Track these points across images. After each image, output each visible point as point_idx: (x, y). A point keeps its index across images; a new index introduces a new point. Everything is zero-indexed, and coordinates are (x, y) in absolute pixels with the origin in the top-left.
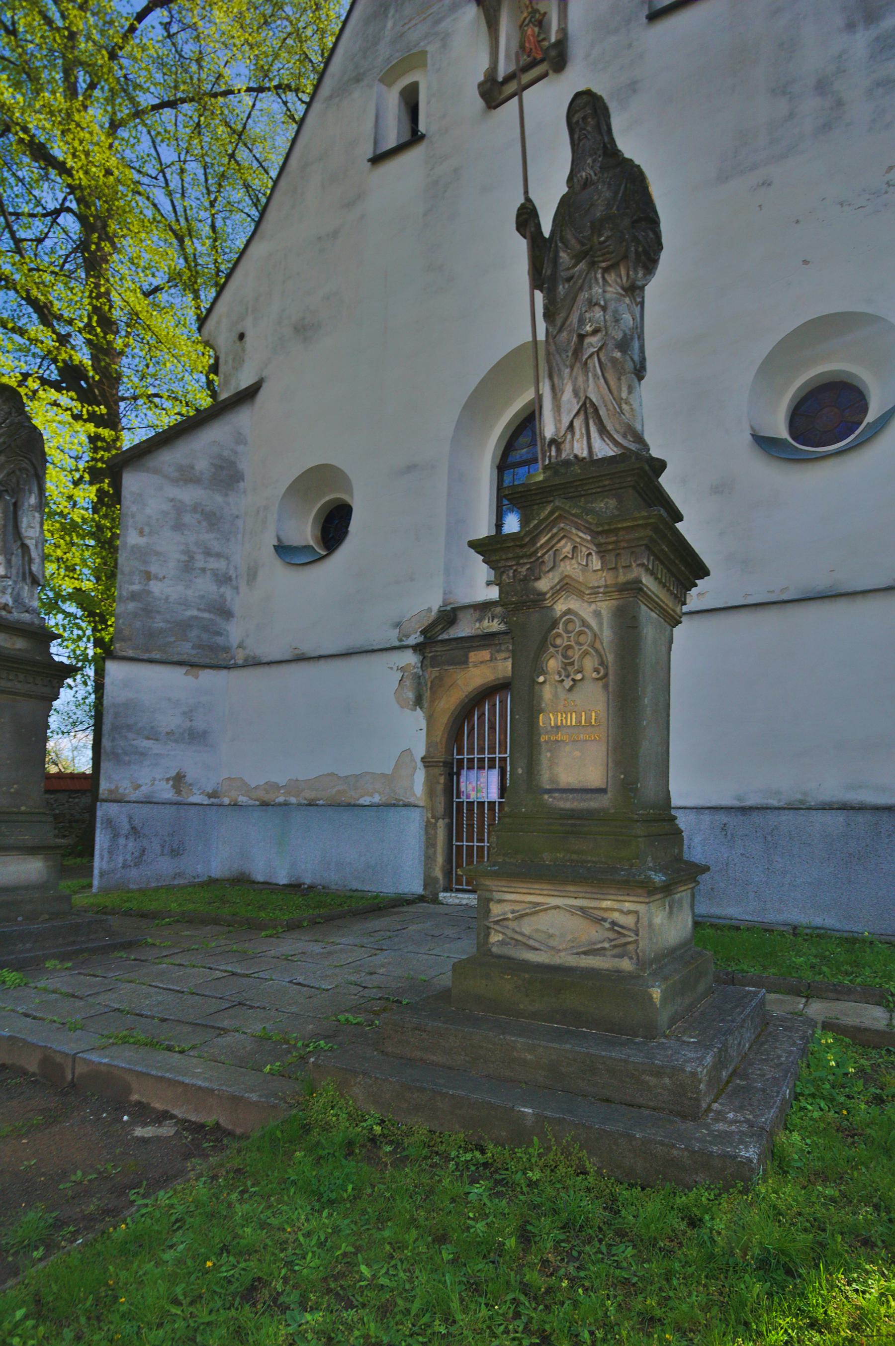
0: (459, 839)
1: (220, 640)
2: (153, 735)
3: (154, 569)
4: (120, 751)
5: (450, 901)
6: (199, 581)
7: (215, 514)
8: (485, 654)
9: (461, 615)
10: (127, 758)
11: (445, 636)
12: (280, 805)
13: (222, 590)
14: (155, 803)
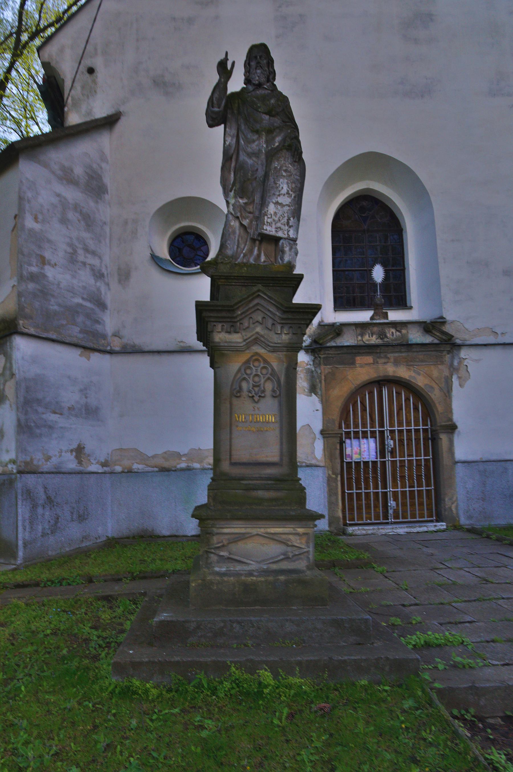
0: (350, 488)
1: (99, 327)
2: (58, 411)
3: (47, 255)
4: (32, 425)
5: (358, 532)
6: (81, 272)
7: (90, 217)
8: (369, 359)
9: (345, 329)
10: (38, 431)
11: (332, 344)
12: (182, 470)
13: (98, 284)
14: (64, 473)
